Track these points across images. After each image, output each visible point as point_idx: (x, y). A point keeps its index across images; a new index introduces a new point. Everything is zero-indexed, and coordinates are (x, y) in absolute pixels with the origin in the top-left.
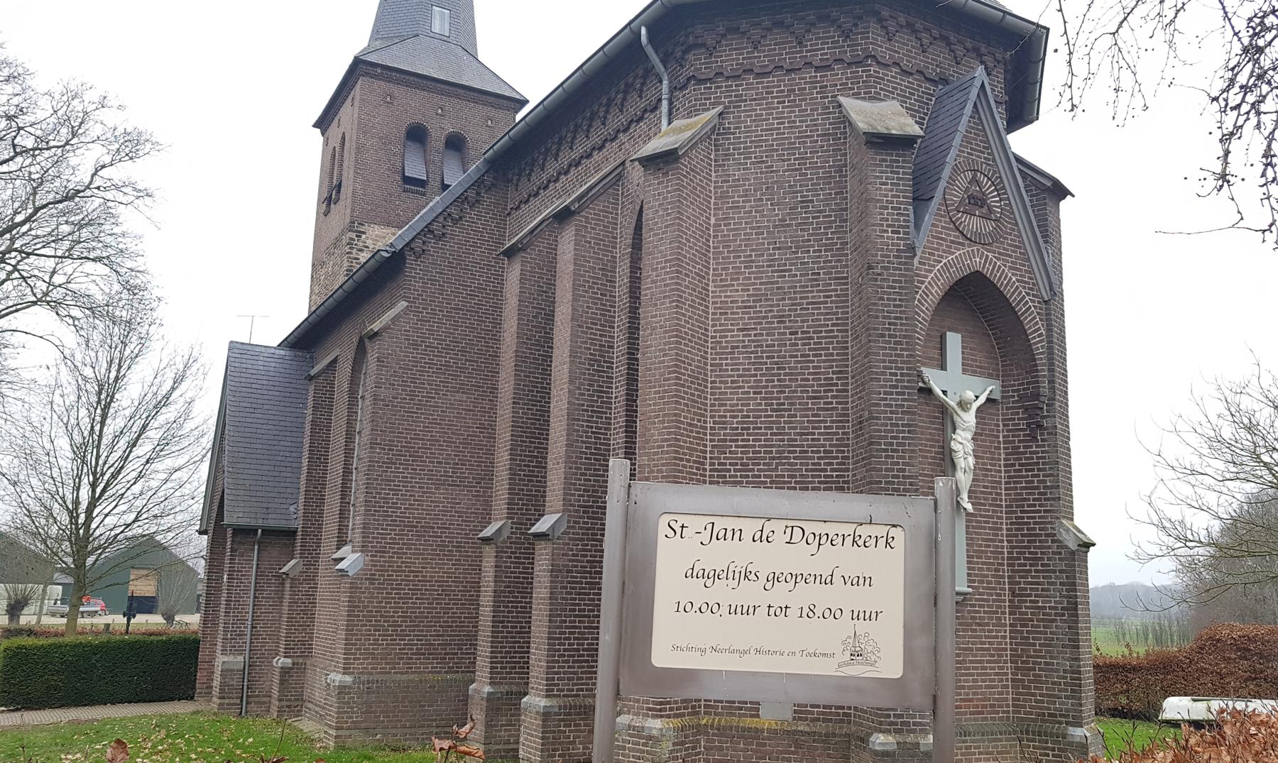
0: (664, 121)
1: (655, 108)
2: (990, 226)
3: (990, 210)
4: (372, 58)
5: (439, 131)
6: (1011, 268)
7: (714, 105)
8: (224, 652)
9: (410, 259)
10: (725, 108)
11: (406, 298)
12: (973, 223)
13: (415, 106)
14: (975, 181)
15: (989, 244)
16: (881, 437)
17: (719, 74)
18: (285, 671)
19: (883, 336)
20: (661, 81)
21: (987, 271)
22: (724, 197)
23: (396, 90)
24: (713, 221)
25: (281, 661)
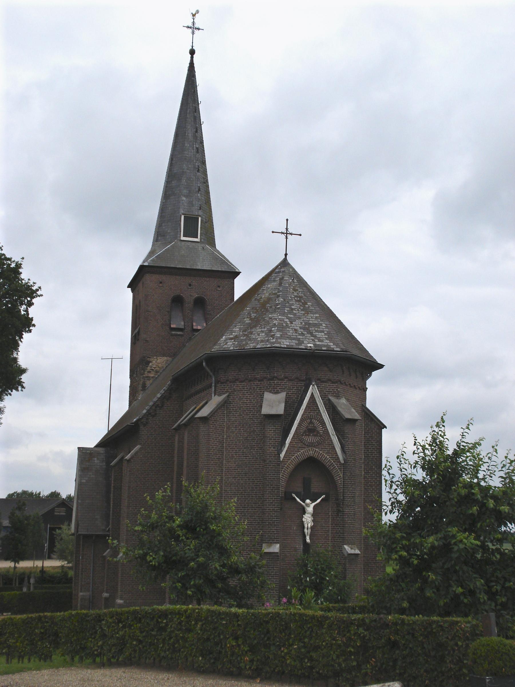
0: (213, 395)
1: (211, 387)
2: (318, 439)
3: (318, 432)
4: (146, 264)
5: (190, 296)
6: (326, 453)
7: (227, 392)
8: (81, 592)
9: (142, 427)
10: (230, 393)
11: (140, 444)
12: (310, 439)
13: (175, 285)
14: (311, 422)
15: (317, 446)
16: (267, 520)
17: (227, 380)
18: (106, 599)
19: (268, 485)
20: (212, 378)
21: (316, 455)
22: (228, 428)
23: (163, 278)
24: (225, 437)
25: (105, 595)
